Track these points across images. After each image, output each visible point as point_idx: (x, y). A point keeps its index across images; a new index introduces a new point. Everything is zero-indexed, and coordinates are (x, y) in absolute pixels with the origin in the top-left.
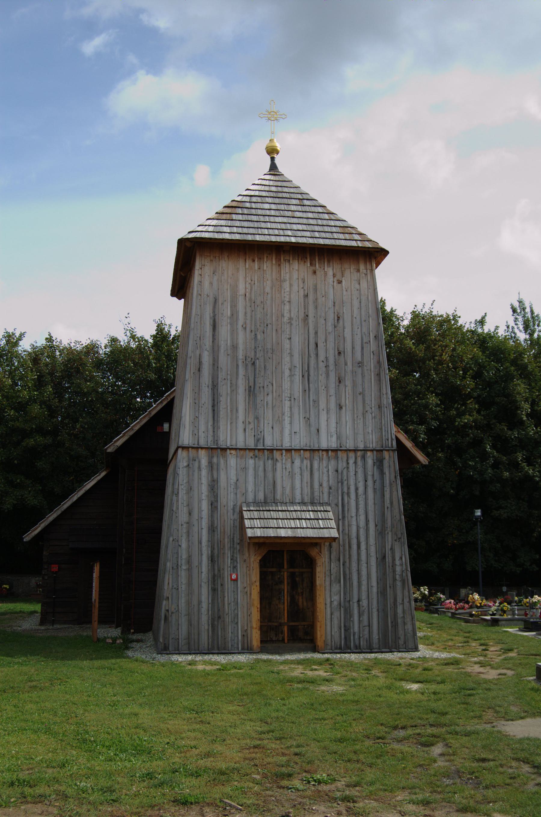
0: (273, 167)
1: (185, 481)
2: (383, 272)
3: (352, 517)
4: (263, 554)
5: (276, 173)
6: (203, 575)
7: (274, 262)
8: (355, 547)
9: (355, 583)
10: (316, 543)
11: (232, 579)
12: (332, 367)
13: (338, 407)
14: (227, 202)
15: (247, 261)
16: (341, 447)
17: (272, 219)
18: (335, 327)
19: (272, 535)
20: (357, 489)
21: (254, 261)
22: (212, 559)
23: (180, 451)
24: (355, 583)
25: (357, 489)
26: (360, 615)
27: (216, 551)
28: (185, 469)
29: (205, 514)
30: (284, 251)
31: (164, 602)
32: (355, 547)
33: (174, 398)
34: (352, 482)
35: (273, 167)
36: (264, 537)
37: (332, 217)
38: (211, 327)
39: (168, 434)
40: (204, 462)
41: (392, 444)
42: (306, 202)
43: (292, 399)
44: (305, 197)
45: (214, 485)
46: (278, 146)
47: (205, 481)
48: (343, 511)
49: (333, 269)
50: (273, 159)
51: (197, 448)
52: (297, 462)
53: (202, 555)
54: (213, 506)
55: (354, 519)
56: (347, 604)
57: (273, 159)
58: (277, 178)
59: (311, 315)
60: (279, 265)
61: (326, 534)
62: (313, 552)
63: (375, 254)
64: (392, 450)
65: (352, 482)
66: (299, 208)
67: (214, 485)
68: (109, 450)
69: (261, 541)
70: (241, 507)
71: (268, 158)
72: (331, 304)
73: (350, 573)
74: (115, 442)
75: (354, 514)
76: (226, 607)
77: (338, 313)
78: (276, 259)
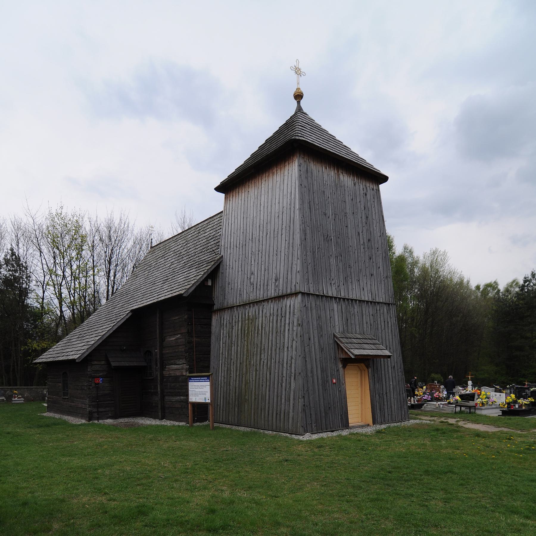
0: (299, 109)
22: (322, 371)
35: (299, 109)
50: (299, 103)
63: (384, 179)
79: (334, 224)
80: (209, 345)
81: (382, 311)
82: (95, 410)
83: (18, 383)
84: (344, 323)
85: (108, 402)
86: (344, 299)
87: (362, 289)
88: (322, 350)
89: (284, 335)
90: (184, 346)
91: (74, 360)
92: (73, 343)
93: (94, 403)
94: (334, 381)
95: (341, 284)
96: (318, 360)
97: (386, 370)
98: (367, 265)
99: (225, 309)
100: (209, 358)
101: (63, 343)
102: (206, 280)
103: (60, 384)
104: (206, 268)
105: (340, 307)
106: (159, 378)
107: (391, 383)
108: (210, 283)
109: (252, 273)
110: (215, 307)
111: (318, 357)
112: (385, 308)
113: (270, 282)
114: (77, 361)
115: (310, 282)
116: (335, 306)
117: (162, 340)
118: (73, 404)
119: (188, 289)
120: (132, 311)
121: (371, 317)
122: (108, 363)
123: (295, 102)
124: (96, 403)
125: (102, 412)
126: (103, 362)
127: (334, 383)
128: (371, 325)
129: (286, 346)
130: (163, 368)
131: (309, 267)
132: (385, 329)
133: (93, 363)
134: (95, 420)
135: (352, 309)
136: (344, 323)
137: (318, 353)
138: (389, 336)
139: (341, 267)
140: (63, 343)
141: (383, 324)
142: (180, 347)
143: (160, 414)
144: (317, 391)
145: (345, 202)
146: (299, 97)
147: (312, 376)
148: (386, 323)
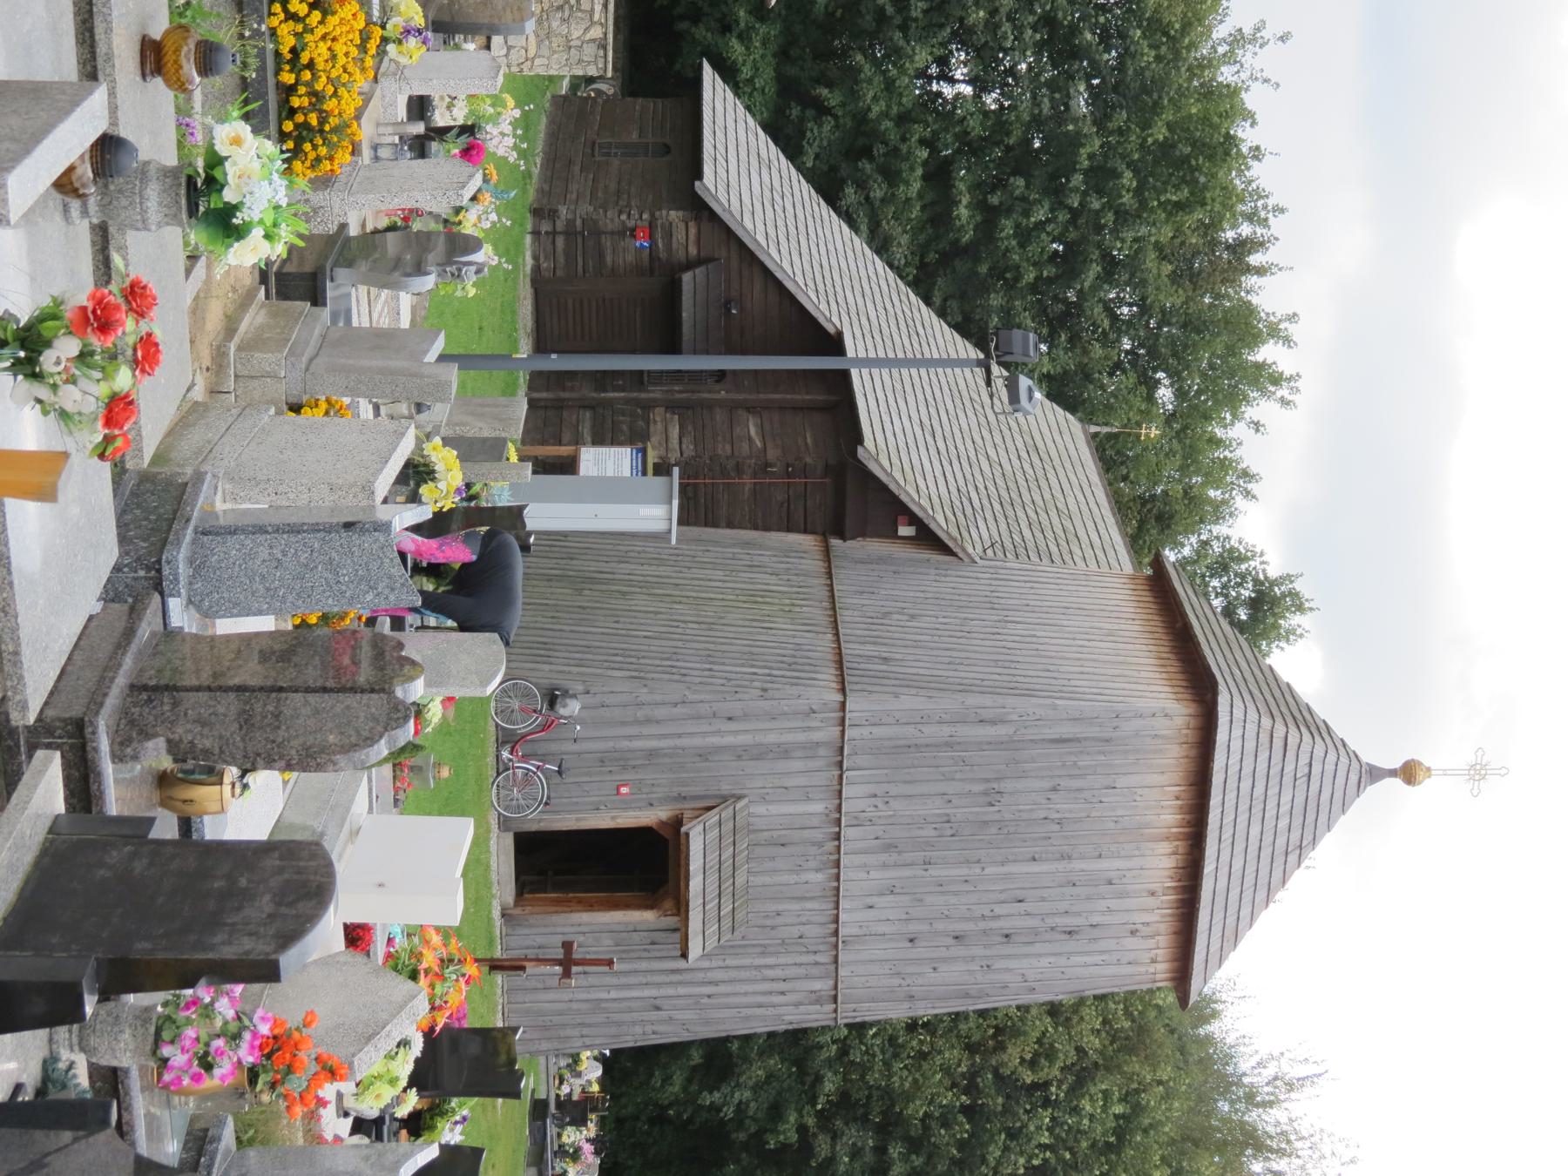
0: (1374, 774)
2: (157, 34)
12: (982, 925)
18: (1052, 929)
21: (1177, 798)
22: (652, 754)
29: (729, 740)
34: (782, 960)
35: (1374, 774)
37: (1261, 895)
39: (894, 535)
45: (784, 752)
50: (1393, 773)
51: (842, 722)
52: (820, 877)
55: (721, 964)
59: (1075, 890)
60: (1168, 839)
62: (668, 904)
65: (782, 960)
67: (784, 752)
75: (729, 962)
77: (1077, 932)
79: (1034, 816)
80: (730, 525)
81: (815, 971)
82: (560, 225)
83: (555, 362)
84: (775, 834)
85: (580, 260)
86: (838, 837)
87: (869, 901)
88: (704, 755)
89: (743, 665)
90: (729, 452)
91: (699, 175)
92: (755, 176)
93: (579, 222)
94: (624, 790)
95: (878, 830)
96: (678, 742)
97: (650, 978)
98: (939, 926)
99: (829, 561)
100: (696, 524)
101: (773, 158)
102: (914, 520)
103: (635, 136)
104: (940, 522)
105: (815, 821)
106: (644, 395)
107: (614, 994)
108: (905, 531)
109: (913, 617)
110: (835, 542)
111: (685, 742)
112: (823, 986)
113: (884, 649)
114: (697, 183)
115: (875, 730)
116: (818, 807)
117: (751, 409)
118: (577, 169)
119: (877, 461)
120: (840, 334)
121: (796, 931)
122: (689, 265)
123: (1397, 764)
124: (579, 229)
125: (554, 243)
126: (693, 251)
127: (618, 788)
128: (773, 928)
129: (715, 667)
130: (671, 407)
131: (910, 730)
132: (765, 980)
133: (692, 224)
134: (534, 225)
135: (812, 864)
136: (775, 834)
137: (697, 742)
138: (746, 994)
139: (921, 833)
140: (773, 158)
141: (778, 973)
142: (728, 447)
143: (544, 395)
144: (598, 734)
145: (1100, 856)
146: (1409, 773)
147: (637, 722)
148: (781, 986)
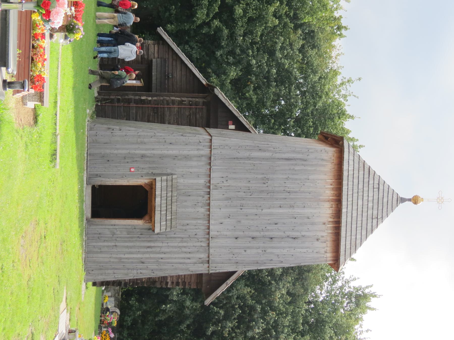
0: (403, 200)
1: (191, 141)
3: (168, 243)
4: (145, 188)
5: (399, 201)
6: (134, 151)
7: (331, 198)
8: (149, 244)
9: (127, 244)
10: (151, 220)
11: (130, 168)
13: (236, 236)
14: (373, 168)
15: (331, 181)
16: (211, 238)
17: (360, 197)
19: (157, 193)
20: (185, 247)
21: (331, 185)
22: (143, 156)
23: (210, 137)
24: (127, 244)
25: (185, 247)
26: (108, 247)
27: (148, 159)
28: (198, 141)
29: (170, 152)
30: (337, 204)
31: (118, 128)
32: (149, 244)
33: (250, 132)
35: (403, 200)
36: (156, 187)
38: (287, 157)
40: (202, 152)
41: (212, 270)
42: (375, 221)
43: (241, 208)
44: (380, 220)
46: (420, 204)
47: (192, 153)
48: (171, 238)
49: (326, 236)
50: (410, 200)
53: (146, 150)
54: (175, 157)
56: (114, 239)
57: (410, 200)
58: (395, 202)
60: (329, 201)
61: (157, 226)
62: (147, 217)
64: (209, 270)
66: (370, 216)
67: (187, 158)
68: (215, 90)
69: (154, 186)
70: (175, 174)
71: (411, 197)
72: (303, 233)
73: (133, 242)
74: (221, 94)
76: (114, 165)
78: (333, 199)
